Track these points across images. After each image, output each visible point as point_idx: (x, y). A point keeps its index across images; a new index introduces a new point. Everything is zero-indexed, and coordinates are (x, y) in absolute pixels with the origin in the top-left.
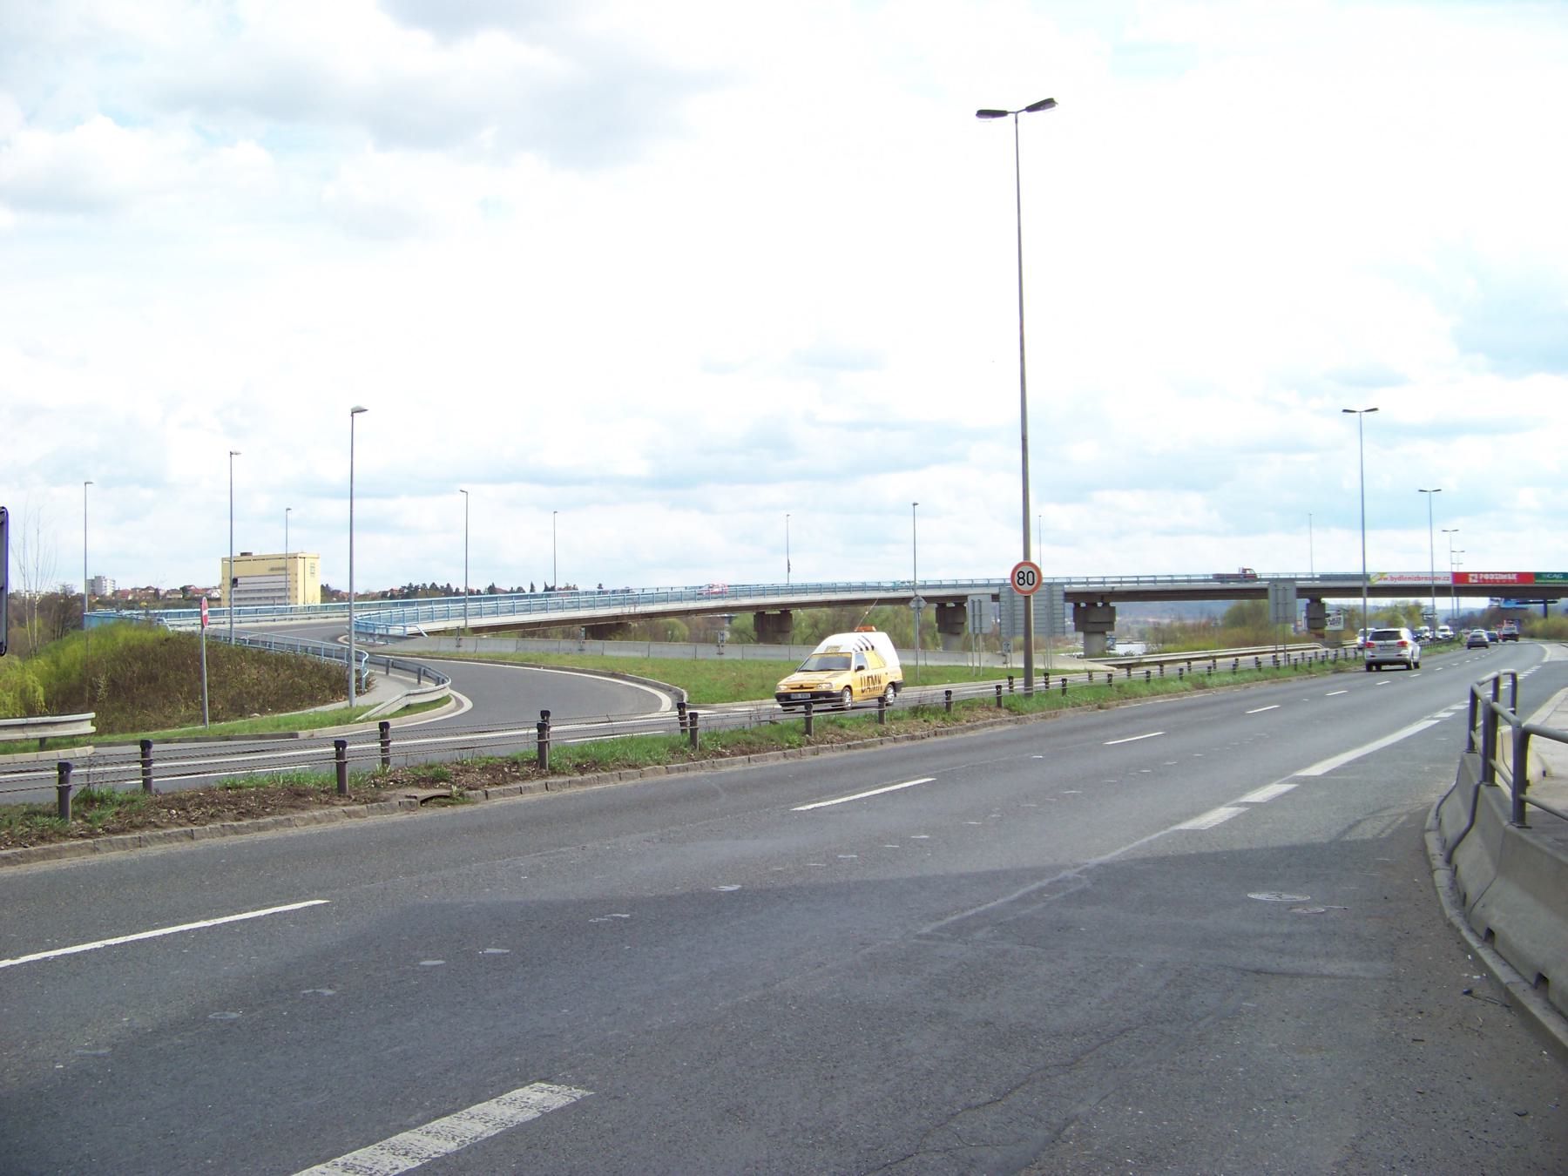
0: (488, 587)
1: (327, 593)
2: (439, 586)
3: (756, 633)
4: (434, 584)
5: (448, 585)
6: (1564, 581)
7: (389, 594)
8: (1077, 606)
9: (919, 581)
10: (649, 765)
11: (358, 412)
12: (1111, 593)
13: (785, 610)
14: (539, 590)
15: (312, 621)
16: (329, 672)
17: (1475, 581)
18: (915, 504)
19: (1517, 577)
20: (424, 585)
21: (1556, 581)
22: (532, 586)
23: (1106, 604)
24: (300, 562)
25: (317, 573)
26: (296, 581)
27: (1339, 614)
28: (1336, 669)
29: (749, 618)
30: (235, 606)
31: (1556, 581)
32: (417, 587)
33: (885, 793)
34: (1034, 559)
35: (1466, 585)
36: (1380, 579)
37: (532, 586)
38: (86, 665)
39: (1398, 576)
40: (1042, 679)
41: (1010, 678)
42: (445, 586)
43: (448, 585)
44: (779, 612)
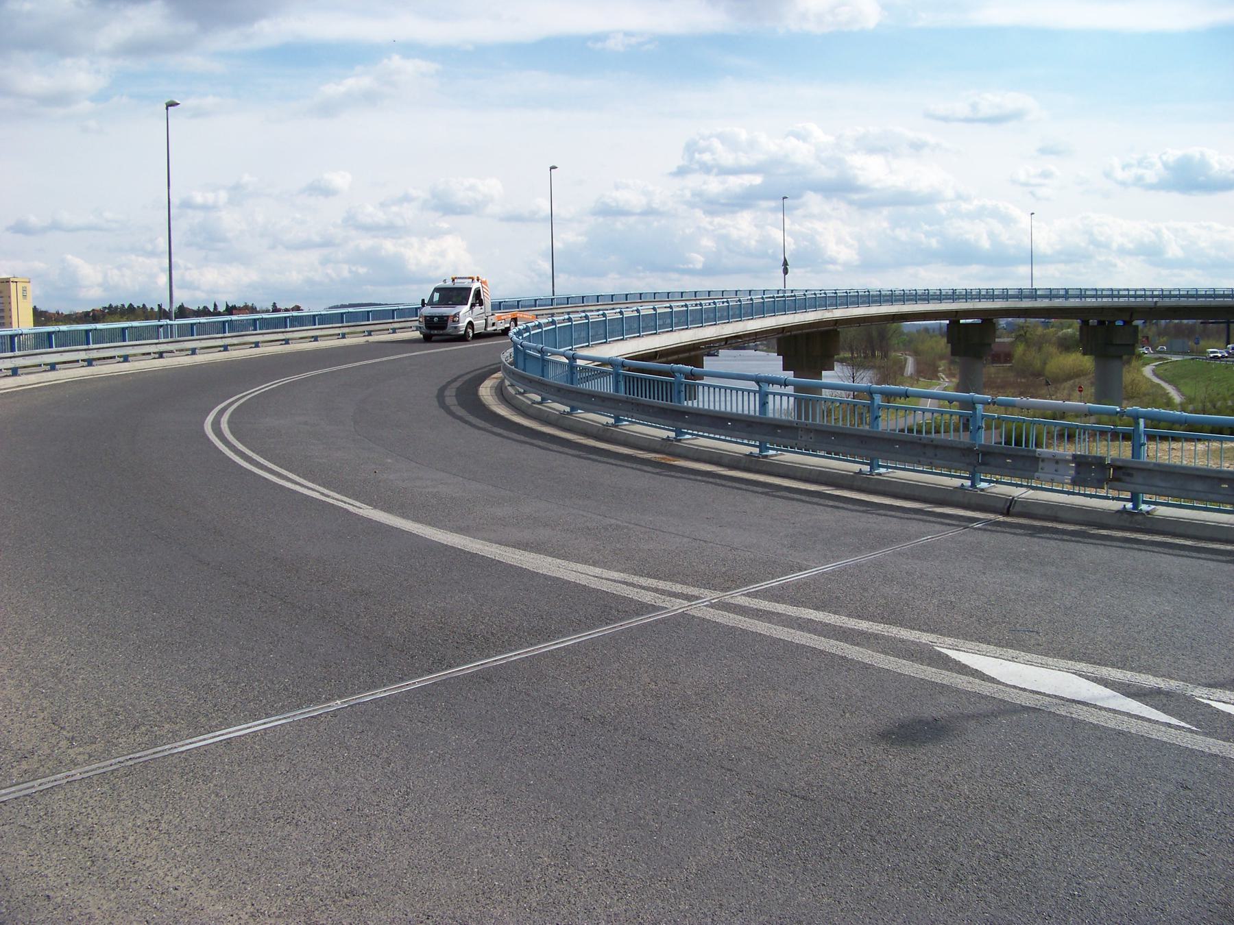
0: (178, 306)
1: (40, 317)
2: (135, 306)
4: (131, 304)
5: (144, 305)
7: (91, 314)
8: (1085, 323)
9: (182, 297)
12: (1151, 308)
13: (988, 318)
14: (222, 309)
15: (375, 338)
16: (1134, 380)
20: (123, 305)
22: (215, 305)
24: (13, 286)
25: (28, 297)
26: (10, 303)
28: (1143, 362)
30: (575, 321)
32: (116, 307)
37: (215, 305)
38: (1134, 380)
42: (141, 306)
43: (144, 305)
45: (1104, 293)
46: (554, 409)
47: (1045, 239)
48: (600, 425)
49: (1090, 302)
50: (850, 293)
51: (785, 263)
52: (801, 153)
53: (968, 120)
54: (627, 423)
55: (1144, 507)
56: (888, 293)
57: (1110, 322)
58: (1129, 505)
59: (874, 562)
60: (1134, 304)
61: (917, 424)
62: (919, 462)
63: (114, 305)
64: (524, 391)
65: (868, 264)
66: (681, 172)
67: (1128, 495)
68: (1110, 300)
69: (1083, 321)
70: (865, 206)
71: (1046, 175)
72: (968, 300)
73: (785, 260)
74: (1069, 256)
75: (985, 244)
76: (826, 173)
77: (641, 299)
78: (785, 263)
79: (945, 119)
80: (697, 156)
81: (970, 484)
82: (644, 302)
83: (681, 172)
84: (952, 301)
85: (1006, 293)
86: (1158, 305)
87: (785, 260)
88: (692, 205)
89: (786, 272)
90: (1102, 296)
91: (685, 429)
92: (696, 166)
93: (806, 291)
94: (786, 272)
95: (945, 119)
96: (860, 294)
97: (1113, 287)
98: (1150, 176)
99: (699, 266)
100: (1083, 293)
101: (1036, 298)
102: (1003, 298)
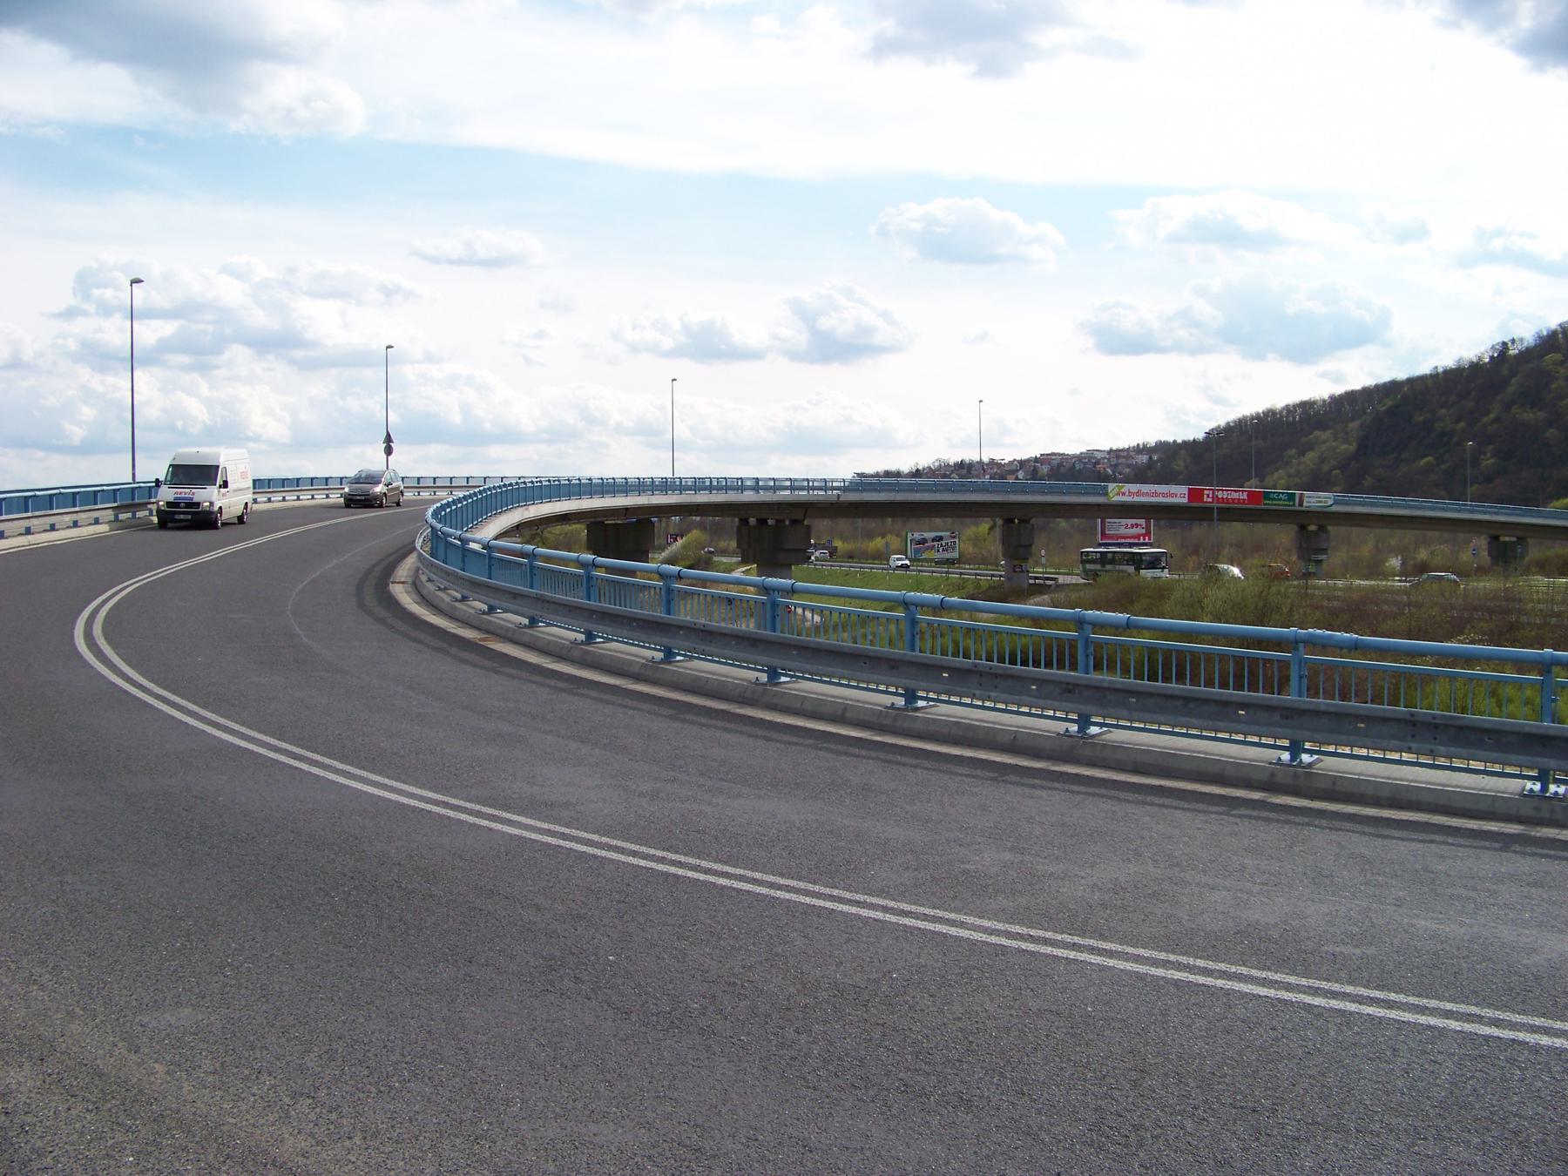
3: (1489, 558)
6: (1288, 503)
8: (745, 521)
10: (1421, 700)
11: (136, 282)
17: (1210, 500)
18: (981, 401)
19: (1248, 495)
21: (1281, 502)
23: (1322, 528)
27: (954, 537)
29: (580, 530)
31: (1281, 502)
33: (308, 749)
34: (385, 456)
35: (1201, 505)
36: (1118, 494)
39: (366, 478)
40: (838, 614)
41: (840, 613)
44: (1514, 539)
45: (816, 484)
46: (509, 622)
47: (523, 411)
48: (568, 643)
49: (749, 496)
50: (554, 481)
51: (388, 439)
52: (230, 293)
53: (460, 262)
54: (602, 640)
55: (1306, 758)
56: (587, 481)
57: (1021, 521)
58: (1286, 756)
59: (352, 869)
60: (815, 498)
61: (1034, 644)
62: (989, 697)
63: (921, 468)
64: (463, 596)
65: (302, 443)
66: (70, 314)
67: (1286, 743)
68: (823, 493)
69: (757, 520)
70: (310, 366)
71: (540, 335)
72: (669, 492)
73: (388, 435)
74: (557, 435)
75: (457, 418)
76: (260, 319)
77: (341, 484)
78: (388, 439)
79: (435, 260)
80: (96, 292)
81: (1076, 728)
82: (422, 487)
83: (70, 314)
84: (651, 493)
85: (678, 483)
86: (841, 499)
87: (388, 435)
88: (76, 358)
89: (389, 451)
90: (814, 488)
91: (676, 649)
92: (92, 308)
93: (519, 478)
94: (389, 451)
95: (435, 260)
96: (583, 481)
97: (603, 477)
98: (667, 343)
99: (76, 441)
100: (811, 484)
101: (726, 490)
102: (738, 490)
